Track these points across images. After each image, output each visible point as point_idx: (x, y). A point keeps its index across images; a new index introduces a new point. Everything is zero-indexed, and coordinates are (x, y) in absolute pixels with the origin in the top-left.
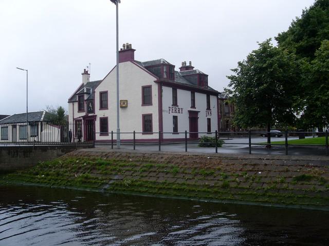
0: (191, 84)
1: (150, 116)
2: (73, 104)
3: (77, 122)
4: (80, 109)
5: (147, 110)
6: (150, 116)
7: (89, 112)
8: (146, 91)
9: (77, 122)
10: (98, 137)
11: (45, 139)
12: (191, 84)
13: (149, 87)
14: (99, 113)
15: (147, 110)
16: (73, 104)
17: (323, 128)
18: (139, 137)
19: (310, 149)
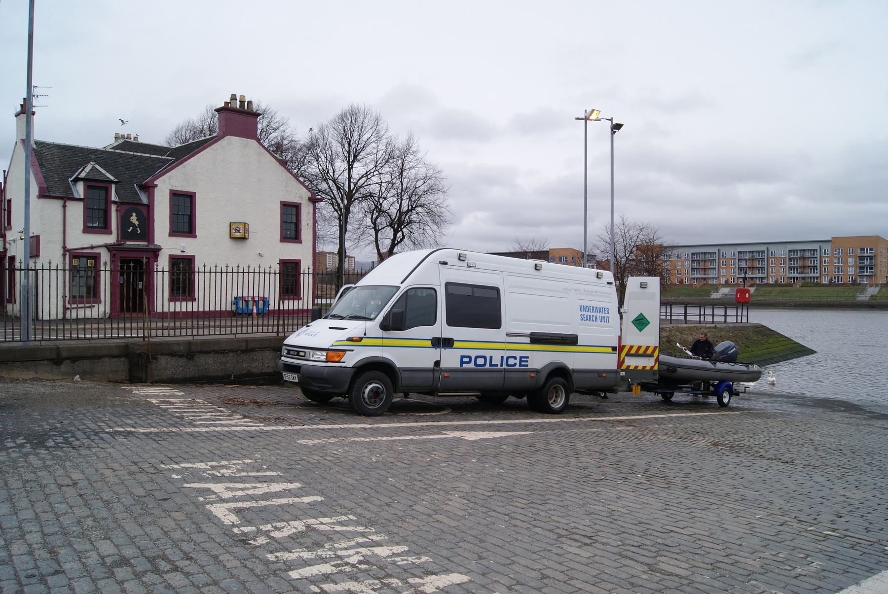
0: (32, 174)
1: (296, 264)
2: (64, 207)
3: (81, 264)
4: (96, 221)
5: (291, 251)
6: (296, 264)
7: (124, 234)
8: (290, 211)
9: (81, 264)
10: (162, 301)
11: (212, 303)
12: (32, 174)
13: (297, 207)
14: (168, 244)
15: (291, 251)
16: (64, 207)
17: (108, 310)
18: (273, 305)
19: (34, 360)
